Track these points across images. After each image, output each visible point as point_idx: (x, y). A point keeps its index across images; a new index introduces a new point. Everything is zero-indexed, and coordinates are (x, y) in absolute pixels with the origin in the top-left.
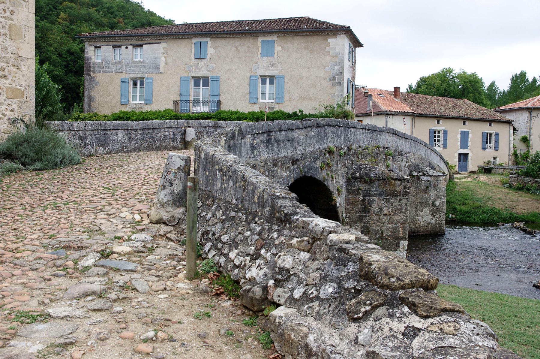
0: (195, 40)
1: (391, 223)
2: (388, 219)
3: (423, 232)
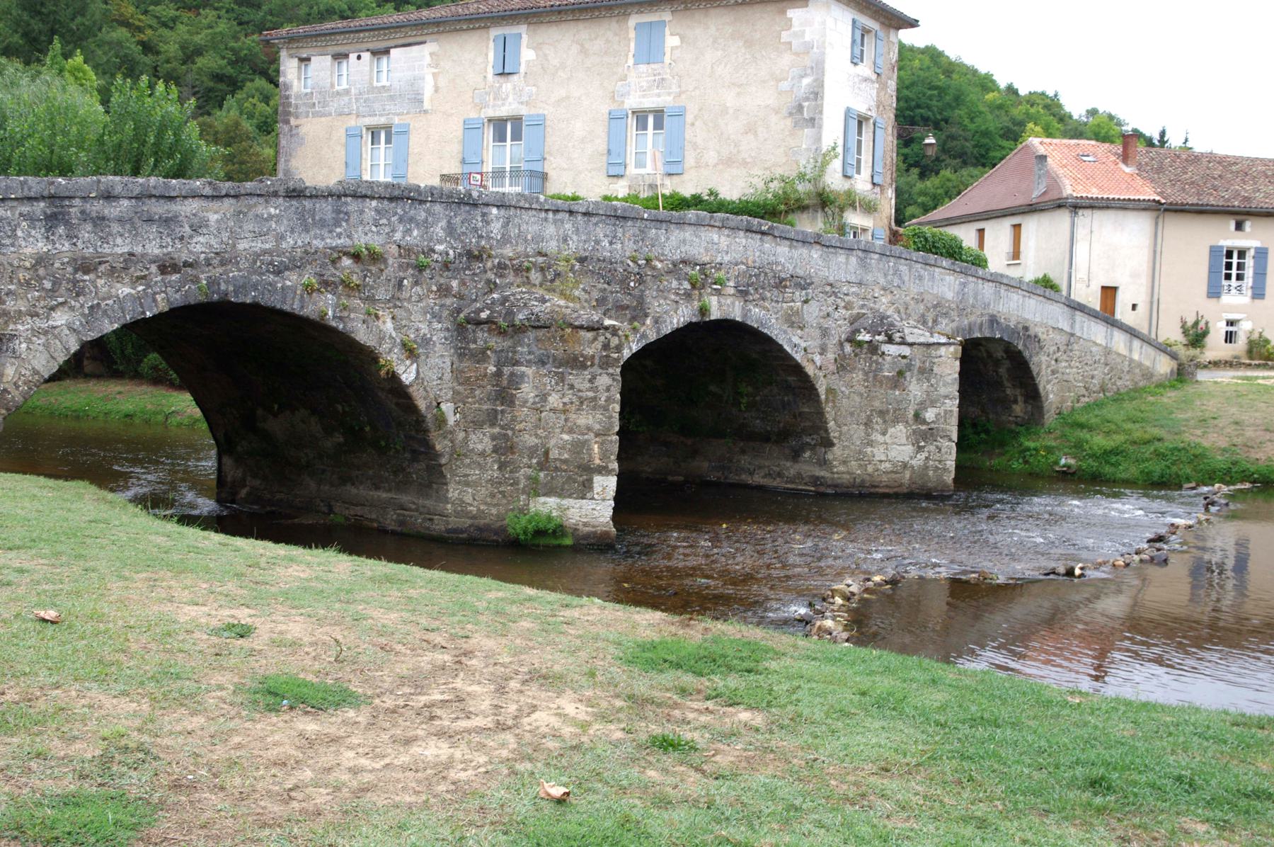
0: (495, 32)
1: (571, 431)
2: (562, 422)
3: (887, 486)
